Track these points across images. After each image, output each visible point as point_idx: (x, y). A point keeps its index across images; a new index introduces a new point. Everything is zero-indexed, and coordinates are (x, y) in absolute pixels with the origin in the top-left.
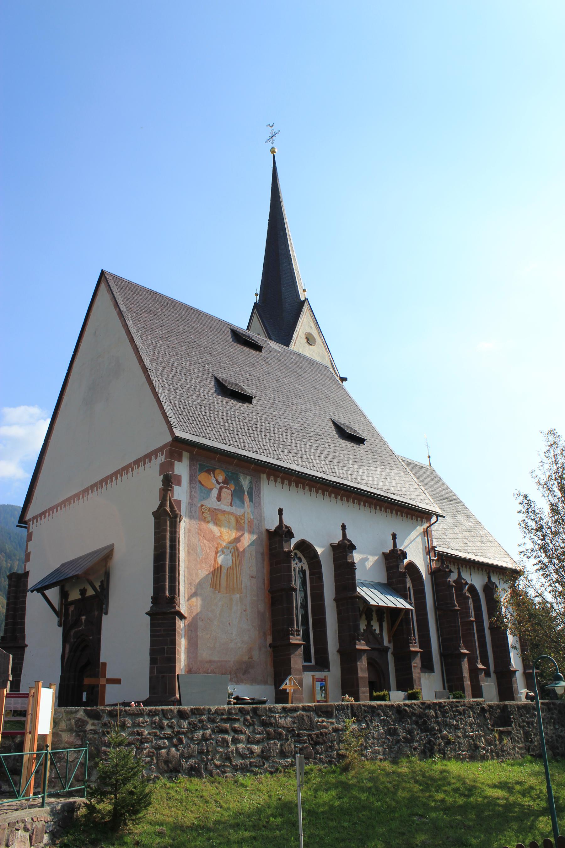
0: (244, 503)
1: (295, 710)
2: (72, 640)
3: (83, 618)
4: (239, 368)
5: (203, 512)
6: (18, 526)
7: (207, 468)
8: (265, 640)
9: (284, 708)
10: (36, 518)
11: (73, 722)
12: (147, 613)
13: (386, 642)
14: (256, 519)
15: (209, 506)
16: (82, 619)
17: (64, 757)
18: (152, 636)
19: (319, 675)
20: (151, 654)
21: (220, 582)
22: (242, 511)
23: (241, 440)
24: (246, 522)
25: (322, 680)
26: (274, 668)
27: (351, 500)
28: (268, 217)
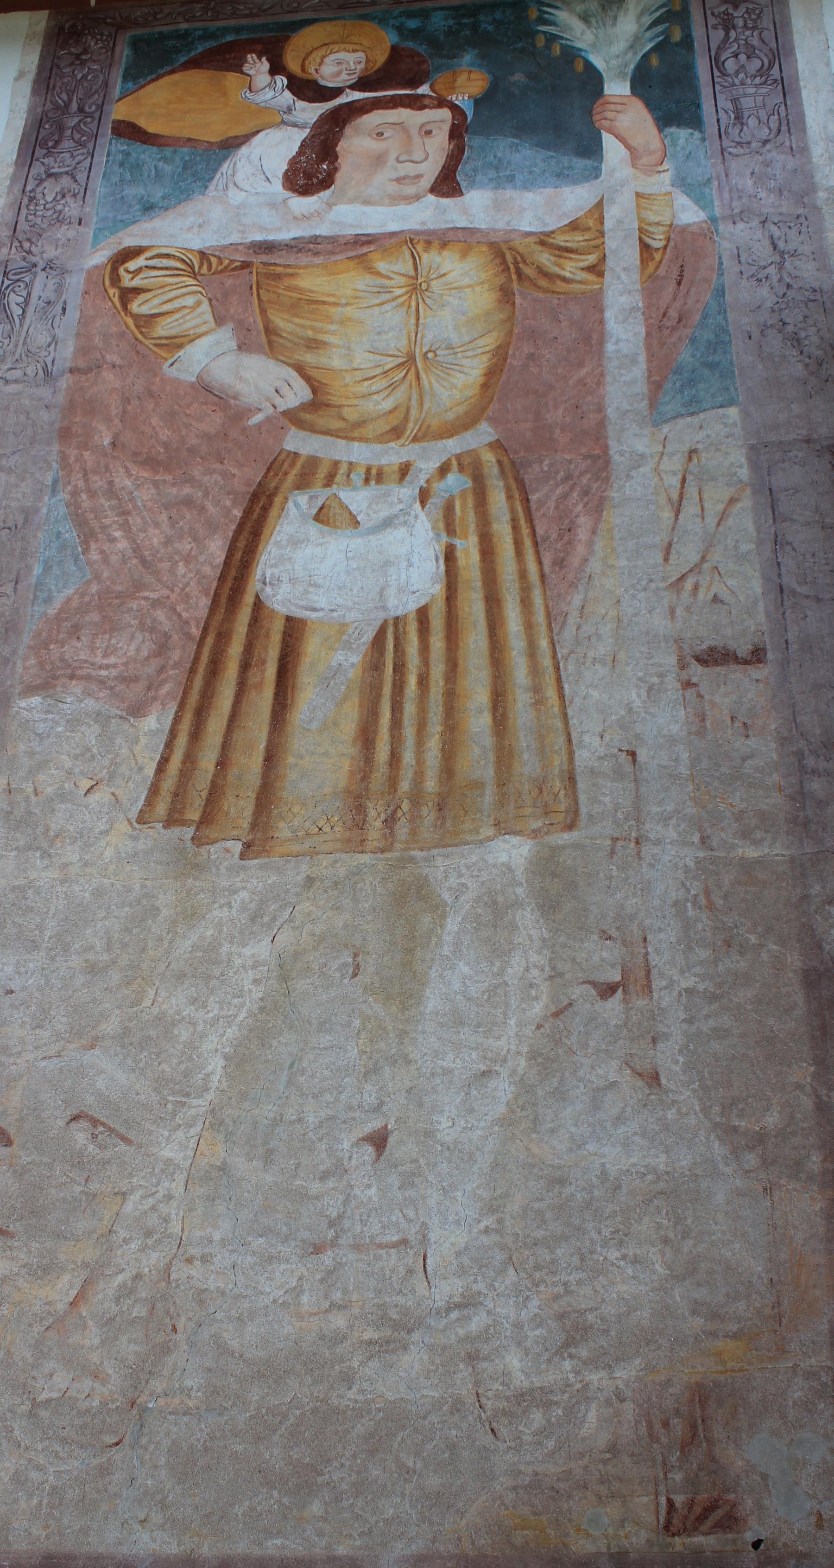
22: (575, 199)
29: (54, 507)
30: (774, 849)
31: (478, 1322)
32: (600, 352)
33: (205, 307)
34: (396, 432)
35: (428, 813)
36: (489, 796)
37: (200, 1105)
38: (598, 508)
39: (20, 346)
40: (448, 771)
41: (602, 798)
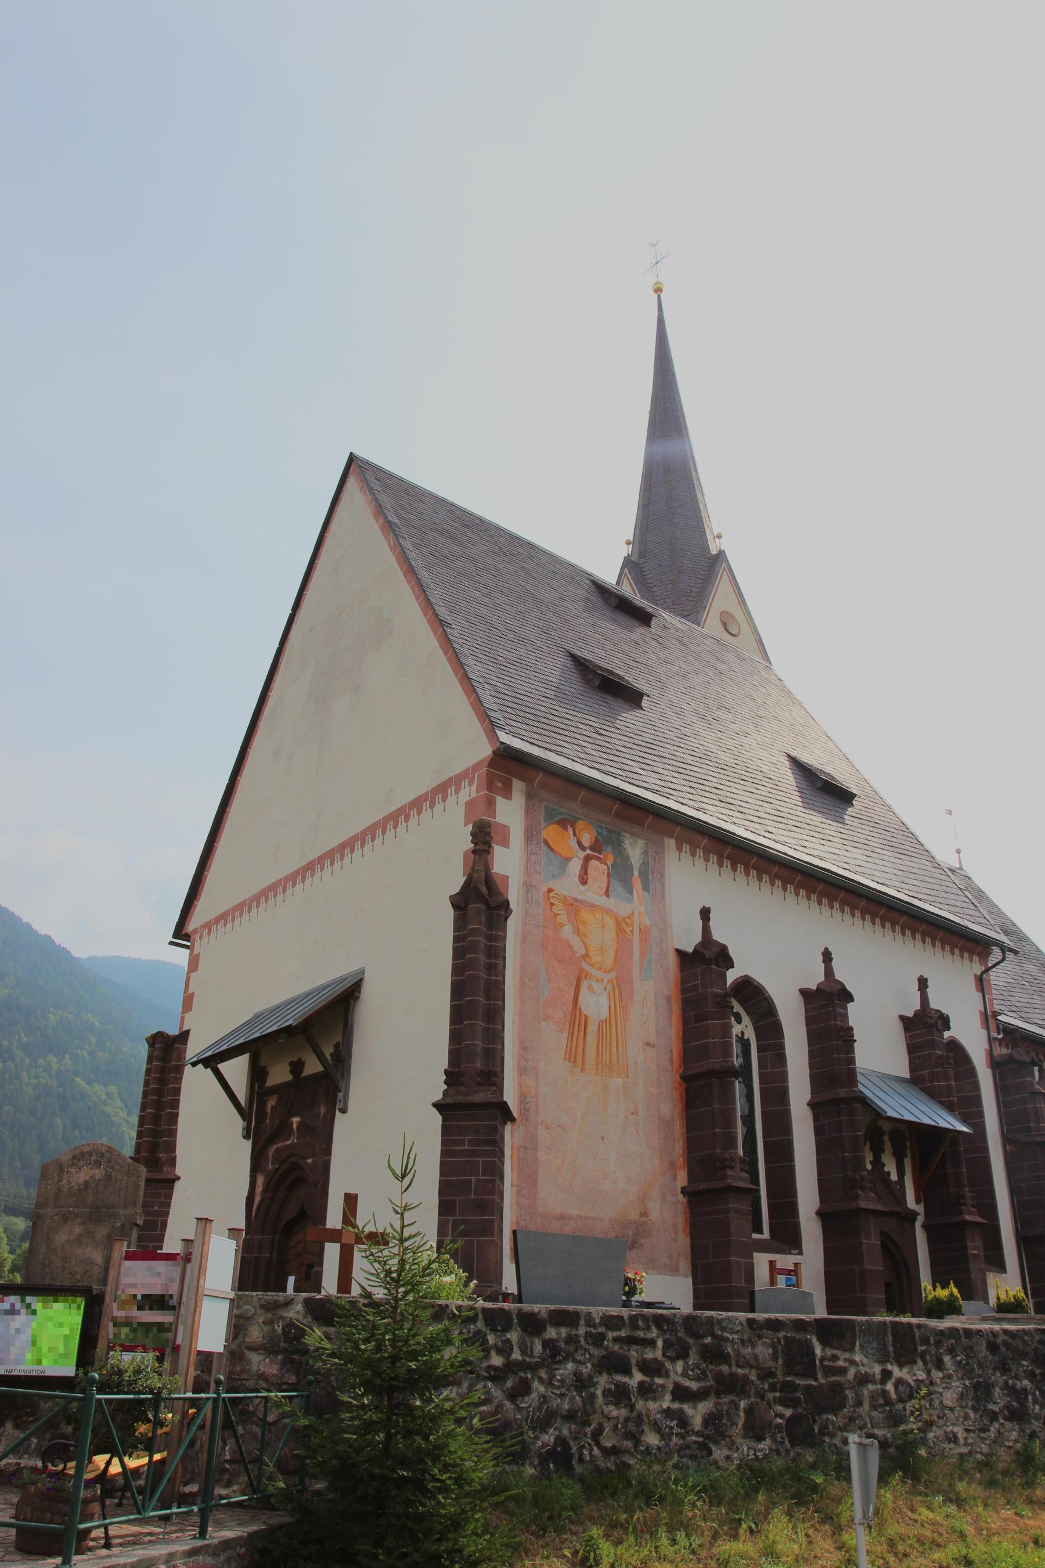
0: (631, 893)
1: (775, 1325)
3: (296, 1120)
4: (614, 647)
5: (552, 904)
6: (171, 943)
7: (559, 817)
8: (675, 1178)
9: (750, 1322)
10: (208, 926)
11: (279, 1328)
12: (435, 1105)
13: (911, 1202)
15: (564, 892)
16: (292, 1124)
17: (254, 1413)
18: (444, 1153)
20: (442, 1193)
21: (584, 1049)
24: (636, 931)
25: (789, 1272)
27: (836, 905)
28: (649, 408)
34: (600, 969)
39: (455, 524)
40: (610, 1060)
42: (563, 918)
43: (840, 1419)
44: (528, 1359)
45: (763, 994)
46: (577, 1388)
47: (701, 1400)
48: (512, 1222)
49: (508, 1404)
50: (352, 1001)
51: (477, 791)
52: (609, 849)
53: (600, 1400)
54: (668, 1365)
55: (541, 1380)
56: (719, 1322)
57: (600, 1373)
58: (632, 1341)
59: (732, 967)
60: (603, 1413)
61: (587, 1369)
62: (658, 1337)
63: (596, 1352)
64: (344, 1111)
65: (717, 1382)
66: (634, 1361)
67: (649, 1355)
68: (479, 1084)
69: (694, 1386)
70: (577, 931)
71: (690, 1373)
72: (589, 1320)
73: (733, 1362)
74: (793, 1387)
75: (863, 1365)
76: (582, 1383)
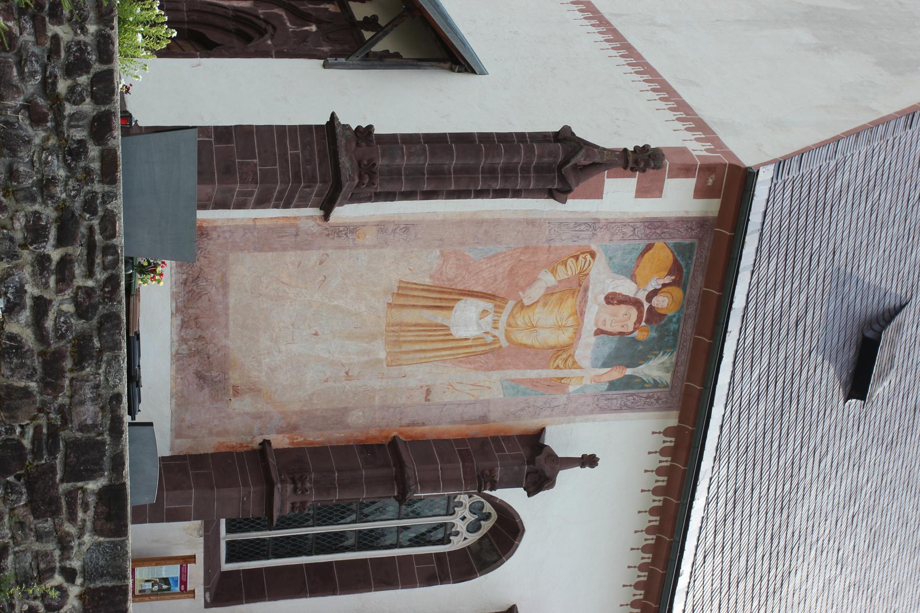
0: (604, 365)
2: (260, 11)
3: (314, 28)
5: (577, 258)
7: (683, 264)
8: (280, 431)
12: (333, 116)
14: (569, 398)
15: (593, 273)
18: (281, 129)
19: (196, 574)
21: (414, 306)
22: (586, 363)
23: (757, 351)
25: (184, 583)
26: (212, 454)
29: (502, 248)
30: (377, 401)
31: (276, 354)
32: (527, 368)
33: (566, 277)
34: (509, 325)
35: (395, 338)
36: (397, 350)
37: (327, 301)
38: (476, 369)
40: (405, 342)
41: (394, 371)
42: (562, 274)
43: (22, 510)
44: (65, 122)
45: (504, 554)
46: (40, 181)
47: (35, 333)
48: (214, 221)
49: (20, 101)
50: (448, 65)
51: (698, 156)
52: (654, 334)
53: (30, 208)
54: (69, 293)
55: (46, 139)
56: (116, 358)
57: (56, 209)
58: (91, 247)
59: (530, 494)
60: (17, 211)
61: (59, 192)
62: (97, 281)
63: (78, 204)
64: (324, 66)
65: (54, 353)
66: (70, 250)
67: (78, 270)
68: (359, 163)
69: (49, 324)
70: (550, 293)
71: (62, 319)
72: (109, 196)
73: (75, 375)
74: (52, 453)
75: (80, 545)
76: (46, 185)
